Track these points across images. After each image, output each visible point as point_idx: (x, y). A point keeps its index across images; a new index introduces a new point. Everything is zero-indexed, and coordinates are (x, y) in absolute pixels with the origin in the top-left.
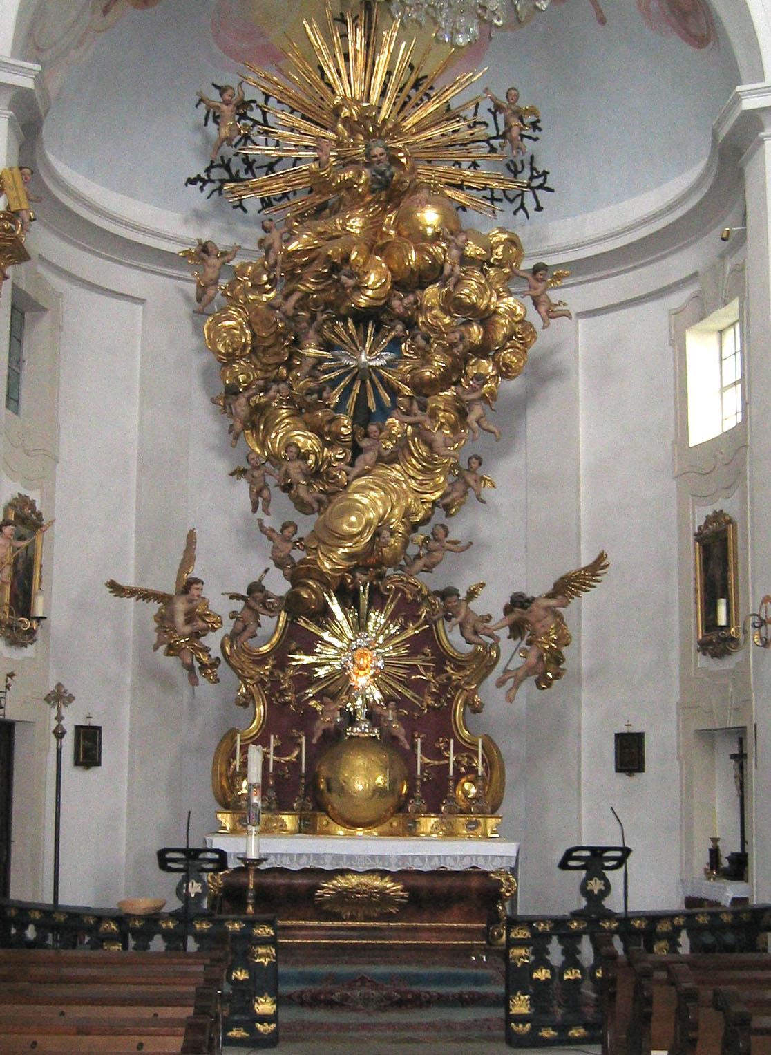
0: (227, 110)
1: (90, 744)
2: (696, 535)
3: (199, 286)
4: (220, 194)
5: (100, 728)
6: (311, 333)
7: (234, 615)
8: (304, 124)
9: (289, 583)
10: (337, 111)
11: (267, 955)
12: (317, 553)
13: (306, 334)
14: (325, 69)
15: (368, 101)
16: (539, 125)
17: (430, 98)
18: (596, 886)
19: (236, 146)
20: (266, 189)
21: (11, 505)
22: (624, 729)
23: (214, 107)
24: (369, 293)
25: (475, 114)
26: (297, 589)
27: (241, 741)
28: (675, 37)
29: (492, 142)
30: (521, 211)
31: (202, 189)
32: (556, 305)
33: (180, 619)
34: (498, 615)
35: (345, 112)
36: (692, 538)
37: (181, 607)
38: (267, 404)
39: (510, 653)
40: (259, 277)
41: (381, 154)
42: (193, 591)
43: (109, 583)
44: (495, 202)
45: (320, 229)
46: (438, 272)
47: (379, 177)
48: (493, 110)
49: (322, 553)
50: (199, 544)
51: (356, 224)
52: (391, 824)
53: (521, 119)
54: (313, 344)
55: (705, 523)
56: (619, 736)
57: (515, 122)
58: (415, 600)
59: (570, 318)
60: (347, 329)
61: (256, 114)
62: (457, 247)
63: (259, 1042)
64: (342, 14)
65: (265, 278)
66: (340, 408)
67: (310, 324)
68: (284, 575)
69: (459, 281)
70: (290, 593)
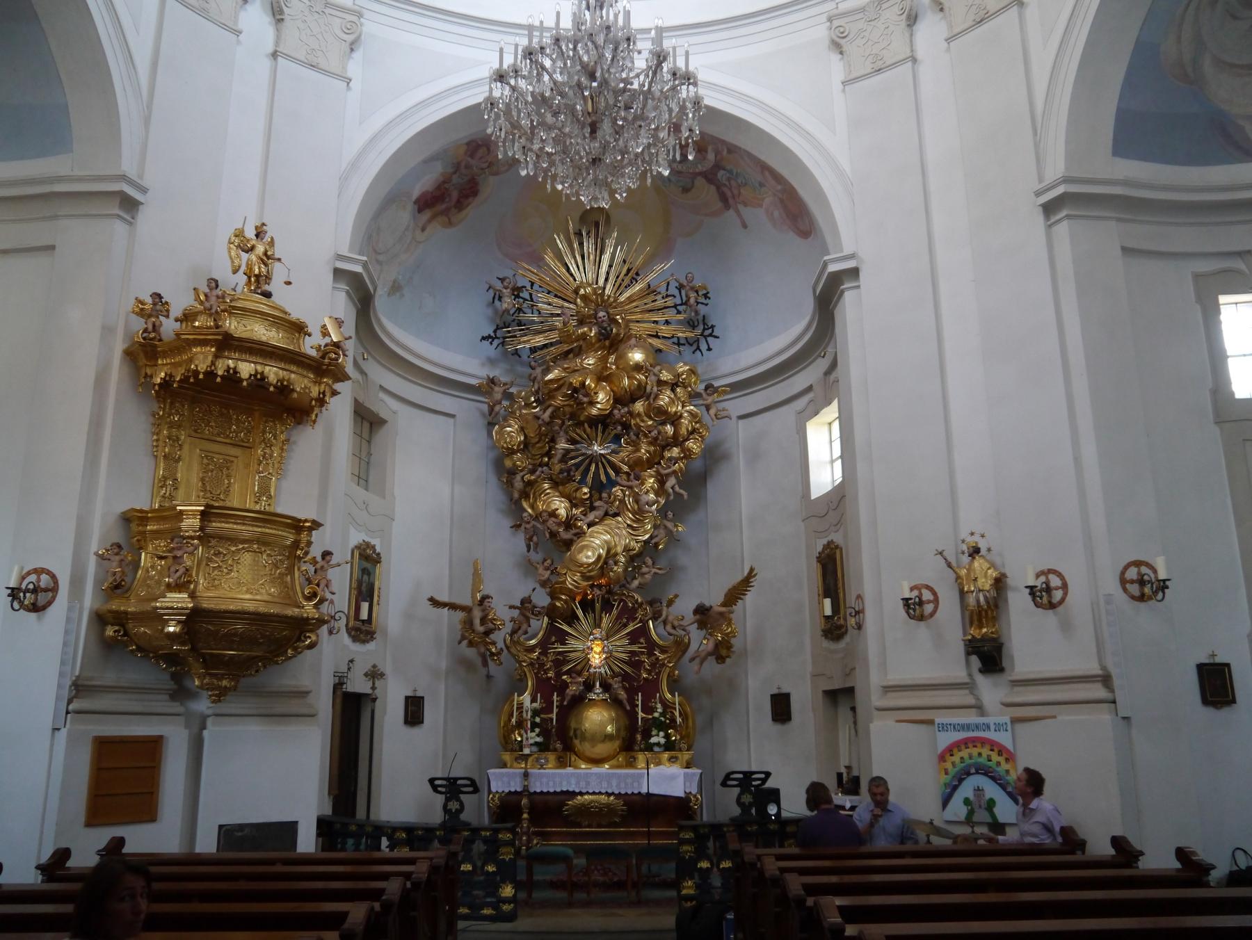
3: (489, 405)
4: (503, 346)
5: (423, 698)
6: (562, 433)
8: (556, 300)
9: (549, 597)
10: (576, 291)
11: (509, 853)
14: (569, 265)
15: (597, 284)
16: (708, 295)
17: (637, 282)
18: (454, 806)
19: (513, 315)
20: (532, 341)
21: (356, 547)
23: (498, 290)
24: (599, 406)
25: (667, 290)
26: (554, 601)
27: (517, 704)
29: (678, 307)
30: (698, 351)
31: (491, 343)
32: (720, 411)
33: (477, 622)
34: (690, 617)
35: (582, 292)
37: (477, 614)
38: (536, 481)
39: (699, 641)
41: (604, 316)
44: (681, 346)
45: (566, 366)
46: (643, 390)
47: (603, 331)
51: (590, 361)
53: (697, 292)
54: (563, 441)
57: (693, 295)
58: (633, 607)
59: (731, 419)
62: (655, 374)
63: (500, 917)
64: (580, 230)
65: (533, 399)
66: (583, 482)
67: (561, 428)
68: (546, 592)
69: (656, 397)
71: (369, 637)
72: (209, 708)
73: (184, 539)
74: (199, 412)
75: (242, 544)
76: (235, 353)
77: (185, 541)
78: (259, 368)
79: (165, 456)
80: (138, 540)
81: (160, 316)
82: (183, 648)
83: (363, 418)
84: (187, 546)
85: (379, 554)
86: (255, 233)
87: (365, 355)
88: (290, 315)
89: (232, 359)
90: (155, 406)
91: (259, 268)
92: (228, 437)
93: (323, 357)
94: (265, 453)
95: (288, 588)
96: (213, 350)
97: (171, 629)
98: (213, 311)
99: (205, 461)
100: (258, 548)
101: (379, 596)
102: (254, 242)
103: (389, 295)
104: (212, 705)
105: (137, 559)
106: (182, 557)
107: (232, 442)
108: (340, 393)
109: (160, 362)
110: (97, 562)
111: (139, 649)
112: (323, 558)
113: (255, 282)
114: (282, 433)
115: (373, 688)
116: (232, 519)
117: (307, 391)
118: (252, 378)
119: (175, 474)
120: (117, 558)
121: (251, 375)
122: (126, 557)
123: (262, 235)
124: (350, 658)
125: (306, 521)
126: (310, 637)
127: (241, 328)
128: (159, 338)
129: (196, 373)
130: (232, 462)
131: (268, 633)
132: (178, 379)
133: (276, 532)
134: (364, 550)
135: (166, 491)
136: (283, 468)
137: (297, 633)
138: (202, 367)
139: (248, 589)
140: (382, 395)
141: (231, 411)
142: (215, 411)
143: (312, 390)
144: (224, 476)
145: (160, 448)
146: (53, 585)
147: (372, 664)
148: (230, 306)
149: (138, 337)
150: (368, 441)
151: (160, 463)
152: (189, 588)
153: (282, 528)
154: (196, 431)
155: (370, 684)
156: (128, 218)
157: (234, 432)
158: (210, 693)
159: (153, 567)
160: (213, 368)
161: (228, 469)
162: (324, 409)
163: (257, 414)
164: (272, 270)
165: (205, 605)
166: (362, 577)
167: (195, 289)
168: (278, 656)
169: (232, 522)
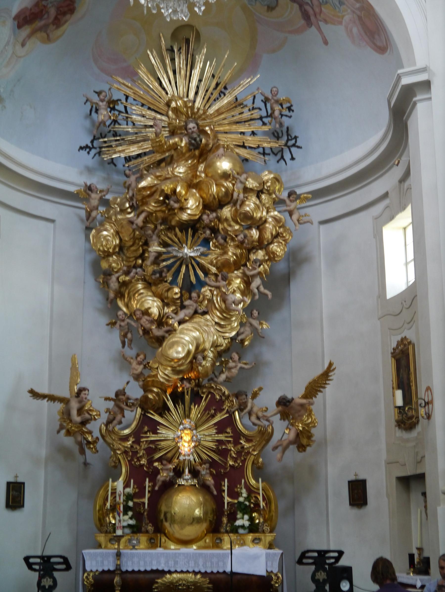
0: (103, 105)
1: (17, 493)
2: (392, 353)
3: (86, 211)
4: (100, 155)
5: (23, 483)
6: (154, 237)
7: (108, 411)
8: (149, 112)
10: (168, 104)
12: (158, 372)
13: (151, 237)
16: (292, 108)
19: (109, 126)
22: (353, 478)
24: (189, 212)
26: (147, 394)
28: (369, 49)
31: (88, 153)
33: (74, 412)
36: (390, 355)
38: (130, 282)
40: (124, 204)
41: (194, 128)
42: (82, 395)
45: (158, 174)
46: (230, 197)
48: (264, 101)
49: (160, 370)
52: (205, 541)
53: (281, 105)
55: (397, 345)
56: (350, 482)
57: (277, 108)
58: (221, 399)
60: (176, 235)
61: (120, 107)
62: (241, 182)
65: (127, 205)
66: (174, 282)
67: (153, 231)
68: (140, 386)
69: (243, 203)
70: (143, 396)
125: (74, 191)
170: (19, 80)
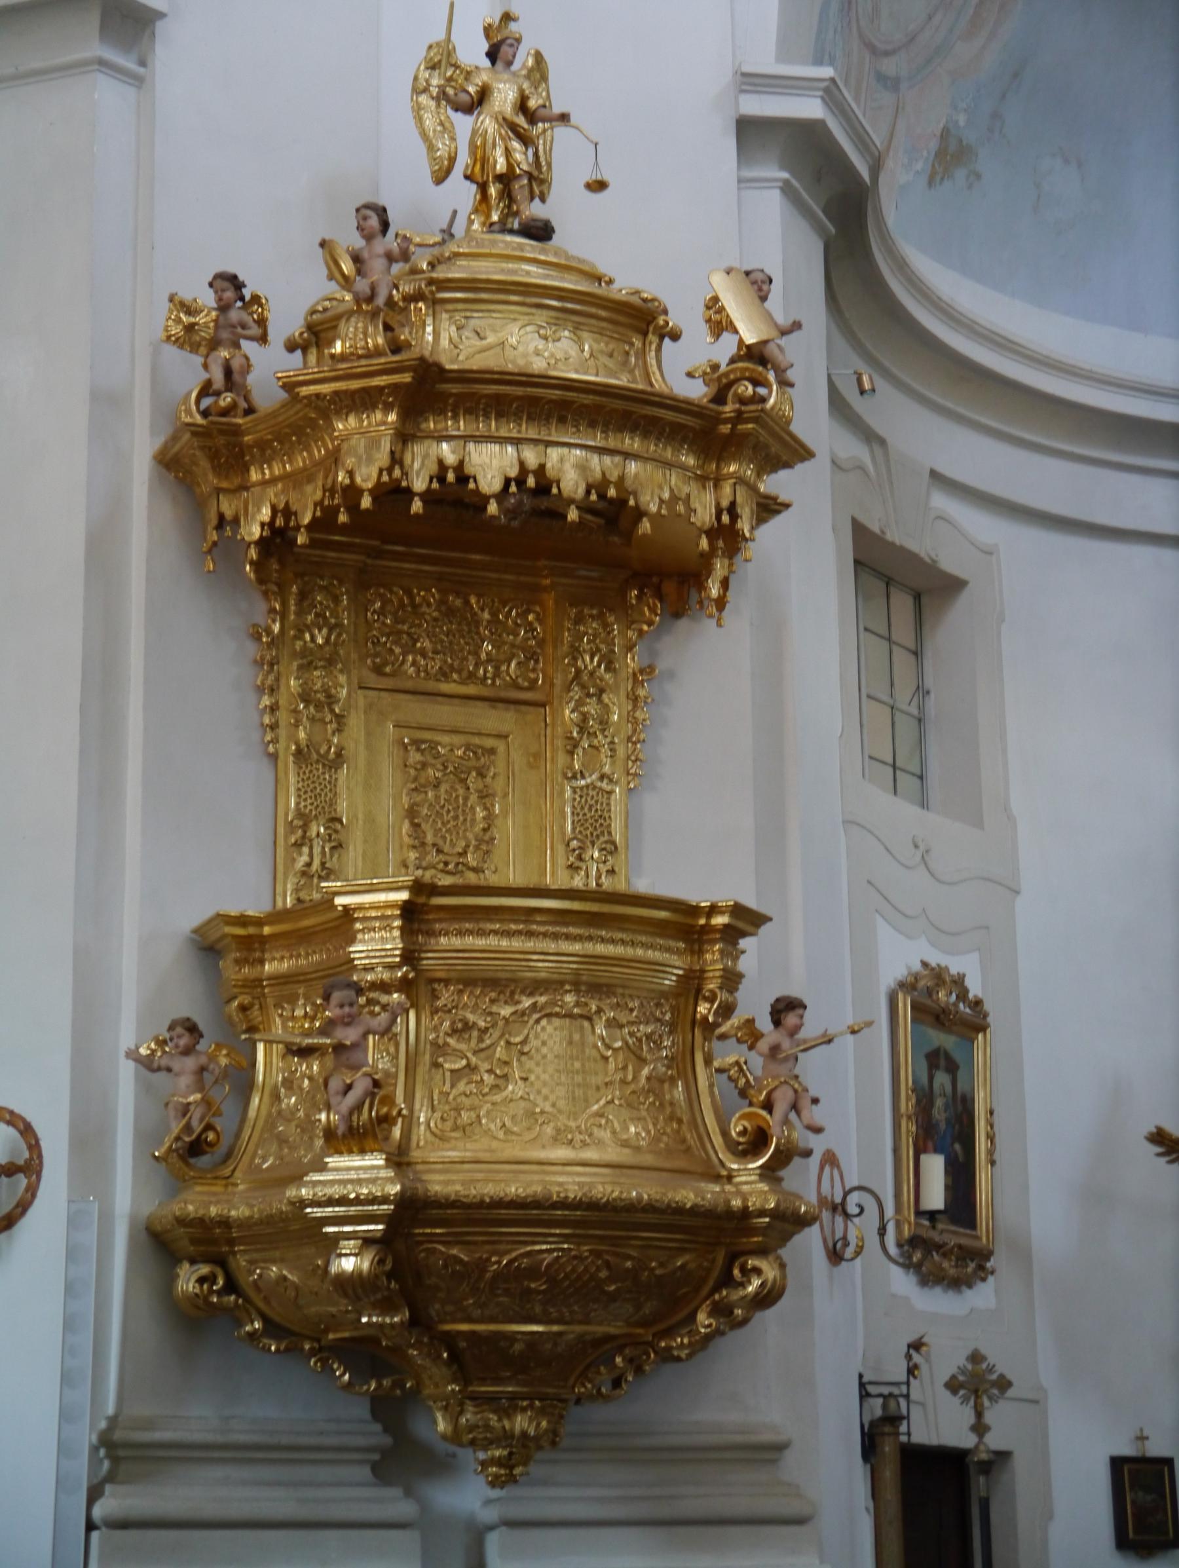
1: (1149, 1498)
5: (1169, 1462)
21: (902, 985)
43: (1152, 1134)
50: (457, 217)
71: (972, 1266)
72: (488, 1502)
73: (360, 991)
74: (382, 612)
75: (531, 994)
76: (455, 417)
77: (362, 1000)
78: (531, 457)
79: (299, 752)
80: (243, 1008)
81: (243, 342)
82: (388, 1320)
83: (889, 582)
84: (372, 1013)
85: (978, 1003)
86: (485, 47)
87: (865, 379)
88: (610, 282)
89: (449, 438)
90: (259, 610)
91: (508, 153)
92: (472, 676)
93: (719, 398)
94: (585, 717)
95: (680, 1121)
96: (392, 417)
97: (348, 1264)
98: (380, 300)
99: (415, 757)
100: (577, 1004)
101: (991, 1138)
102: (484, 77)
103: (931, 183)
104: (496, 1493)
105: (245, 1064)
106: (359, 1045)
107: (485, 692)
108: (787, 506)
109: (254, 476)
110: (138, 1077)
111: (273, 1328)
112: (777, 1023)
113: (501, 196)
114: (630, 648)
115: (980, 1428)
116: (491, 921)
117: (681, 508)
118: (513, 488)
119: (332, 803)
120: (190, 1063)
121: (507, 481)
122: (213, 1058)
123: (505, 49)
124: (912, 1337)
125: (713, 910)
126: (758, 1271)
127: (470, 343)
128: (245, 405)
129: (352, 492)
130: (492, 751)
131: (629, 1264)
132: (306, 520)
133: (629, 952)
134: (930, 992)
135: (311, 855)
136: (641, 756)
137: (720, 1257)
138: (367, 477)
139: (558, 1131)
140: (941, 501)
141: (473, 600)
142: (429, 605)
143: (695, 504)
144: (473, 798)
145: (282, 732)
146: (26, 1155)
147: (968, 1352)
148: (431, 282)
149: (188, 412)
150: (915, 653)
151: (286, 774)
152: (387, 1138)
153: (644, 939)
154: (378, 670)
155: (967, 1415)
156: (130, 64)
157: (489, 660)
158: (481, 1455)
159: (289, 1083)
160: (397, 473)
161: (481, 775)
162: (738, 559)
163: (550, 600)
164: (549, 152)
165: (437, 1188)
166: (931, 1078)
167: (323, 244)
168: (669, 1333)
169: (495, 932)
170: (1016, 75)
